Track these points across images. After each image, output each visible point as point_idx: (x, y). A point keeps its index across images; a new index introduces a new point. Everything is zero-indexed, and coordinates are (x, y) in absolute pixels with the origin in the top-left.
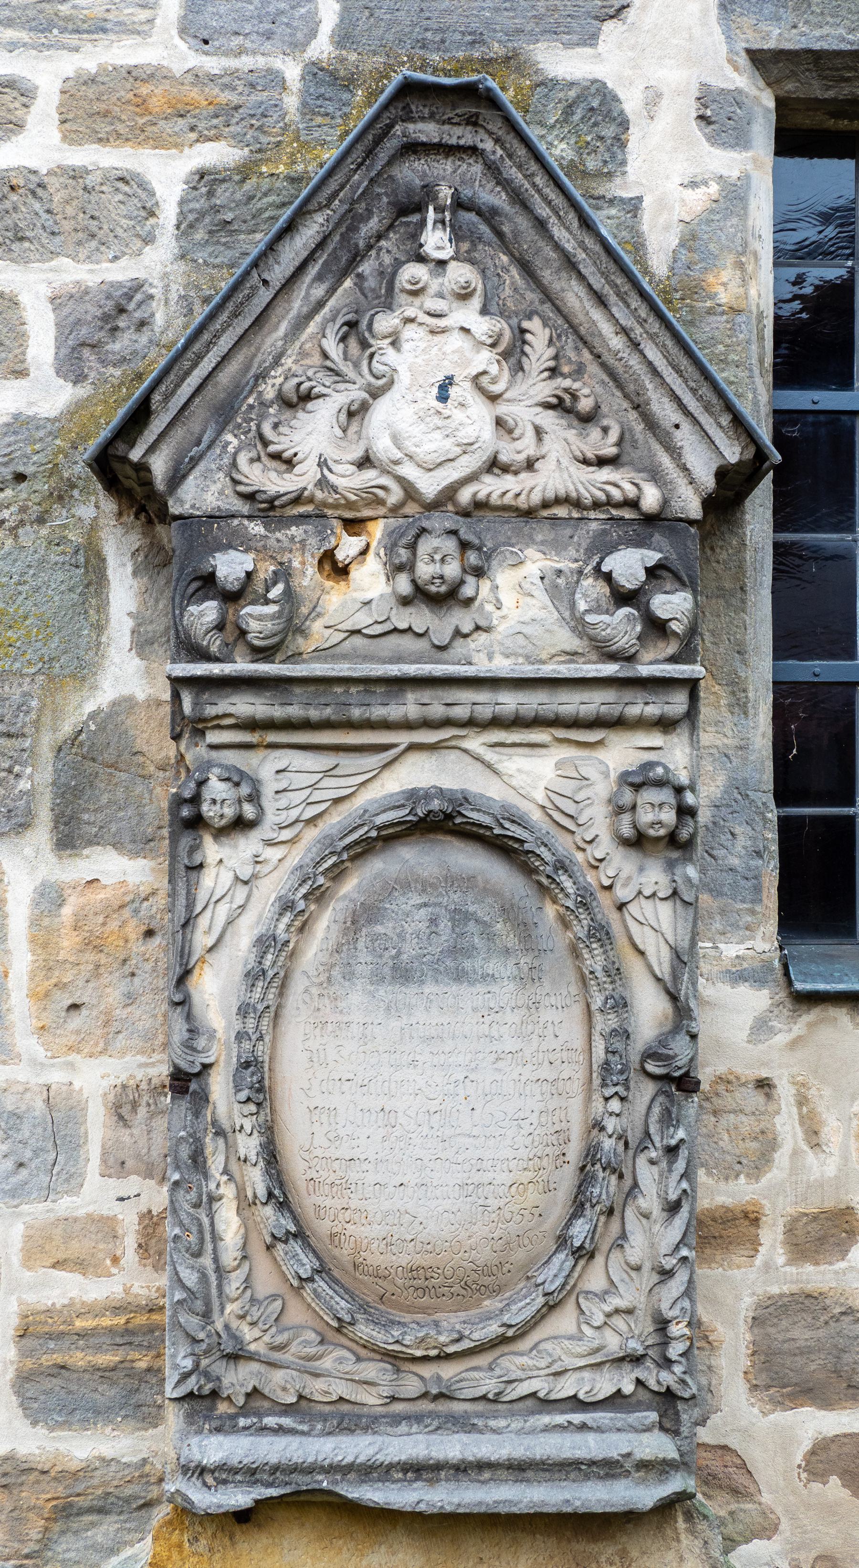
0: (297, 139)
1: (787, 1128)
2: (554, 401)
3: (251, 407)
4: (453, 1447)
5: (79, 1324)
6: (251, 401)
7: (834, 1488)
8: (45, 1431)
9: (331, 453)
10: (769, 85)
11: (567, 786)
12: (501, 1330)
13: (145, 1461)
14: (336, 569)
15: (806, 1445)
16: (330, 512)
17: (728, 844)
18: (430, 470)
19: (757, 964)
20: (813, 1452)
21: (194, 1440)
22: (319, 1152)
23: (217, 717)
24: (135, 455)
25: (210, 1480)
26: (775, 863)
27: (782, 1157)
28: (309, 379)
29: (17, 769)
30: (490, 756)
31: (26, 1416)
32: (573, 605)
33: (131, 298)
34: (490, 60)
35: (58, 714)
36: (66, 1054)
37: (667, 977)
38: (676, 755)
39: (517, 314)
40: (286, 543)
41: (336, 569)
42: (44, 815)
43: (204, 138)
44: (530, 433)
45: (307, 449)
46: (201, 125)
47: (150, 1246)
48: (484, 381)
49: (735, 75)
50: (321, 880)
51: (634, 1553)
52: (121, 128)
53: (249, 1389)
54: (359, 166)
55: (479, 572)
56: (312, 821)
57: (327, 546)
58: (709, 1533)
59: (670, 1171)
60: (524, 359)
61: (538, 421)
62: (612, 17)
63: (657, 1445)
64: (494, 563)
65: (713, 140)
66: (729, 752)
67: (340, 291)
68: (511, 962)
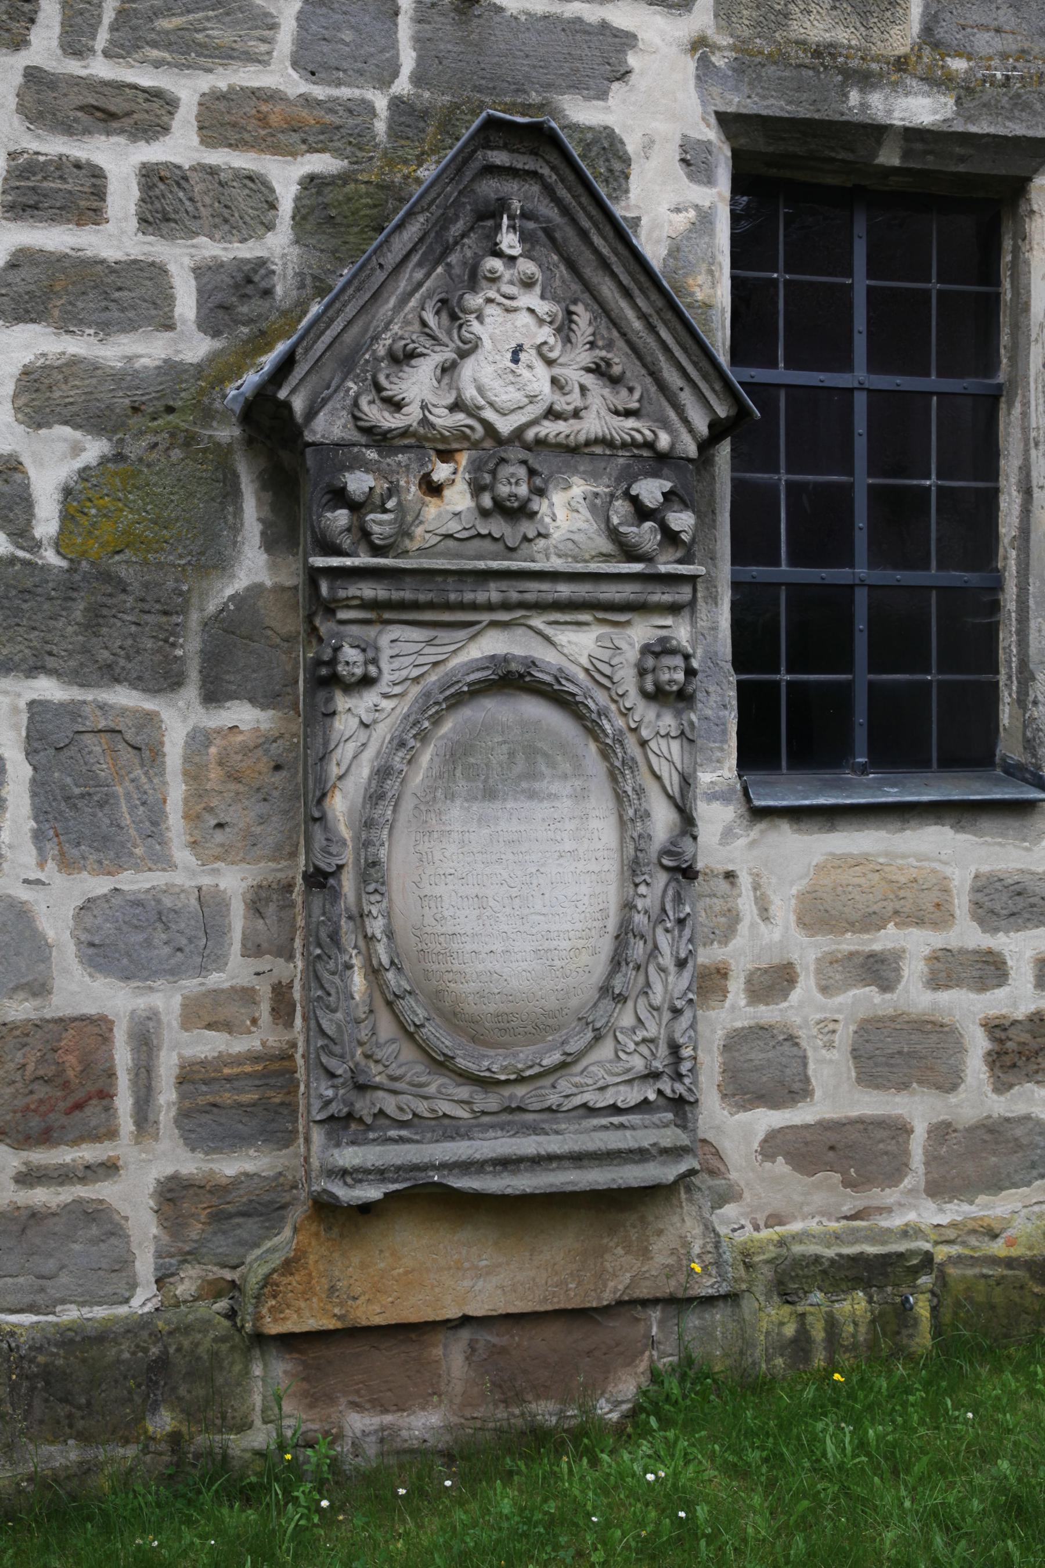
0: (385, 154)
1: (747, 907)
2: (593, 366)
3: (367, 361)
4: (529, 1145)
5: (227, 1071)
6: (367, 356)
7: (781, 1166)
8: (201, 1156)
9: (430, 398)
10: (728, 138)
11: (605, 655)
12: (563, 1058)
13: (280, 1174)
14: (434, 489)
15: (761, 1136)
16: (427, 445)
17: (704, 699)
18: (505, 415)
19: (725, 788)
20: (765, 1141)
21: (336, 1152)
22: (428, 930)
23: (348, 598)
24: (282, 395)
25: (349, 1180)
26: (734, 714)
27: (743, 928)
28: (413, 342)
29: (172, 639)
30: (549, 631)
31: (186, 1145)
32: (608, 520)
33: (256, 272)
34: (530, 105)
35: (204, 595)
36: (213, 862)
37: (677, 795)
38: (682, 633)
39: (564, 300)
40: (394, 468)
41: (434, 489)
42: (194, 675)
43: (312, 150)
44: (577, 390)
45: (412, 396)
46: (311, 139)
47: (282, 1007)
48: (545, 348)
49: (707, 130)
50: (426, 724)
51: (651, 1218)
52: (246, 136)
53: (376, 1111)
54: (452, 179)
55: (541, 492)
56: (416, 680)
57: (426, 470)
58: (702, 1201)
59: (680, 937)
60: (572, 334)
61: (583, 381)
62: (618, 79)
63: (671, 1137)
64: (551, 486)
65: (691, 177)
66: (708, 631)
67: (434, 275)
68: (569, 784)
